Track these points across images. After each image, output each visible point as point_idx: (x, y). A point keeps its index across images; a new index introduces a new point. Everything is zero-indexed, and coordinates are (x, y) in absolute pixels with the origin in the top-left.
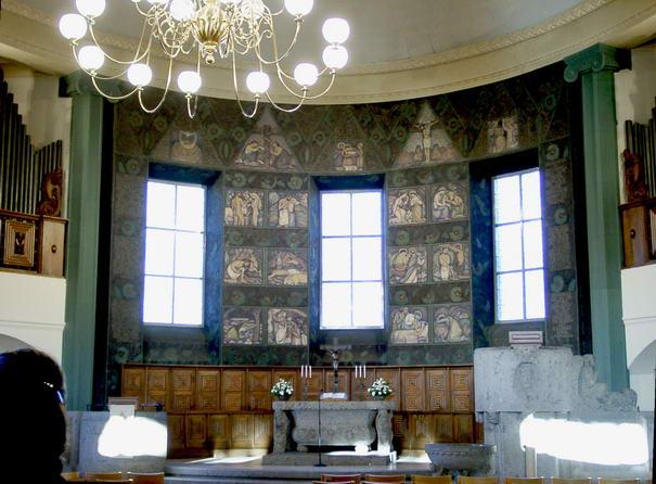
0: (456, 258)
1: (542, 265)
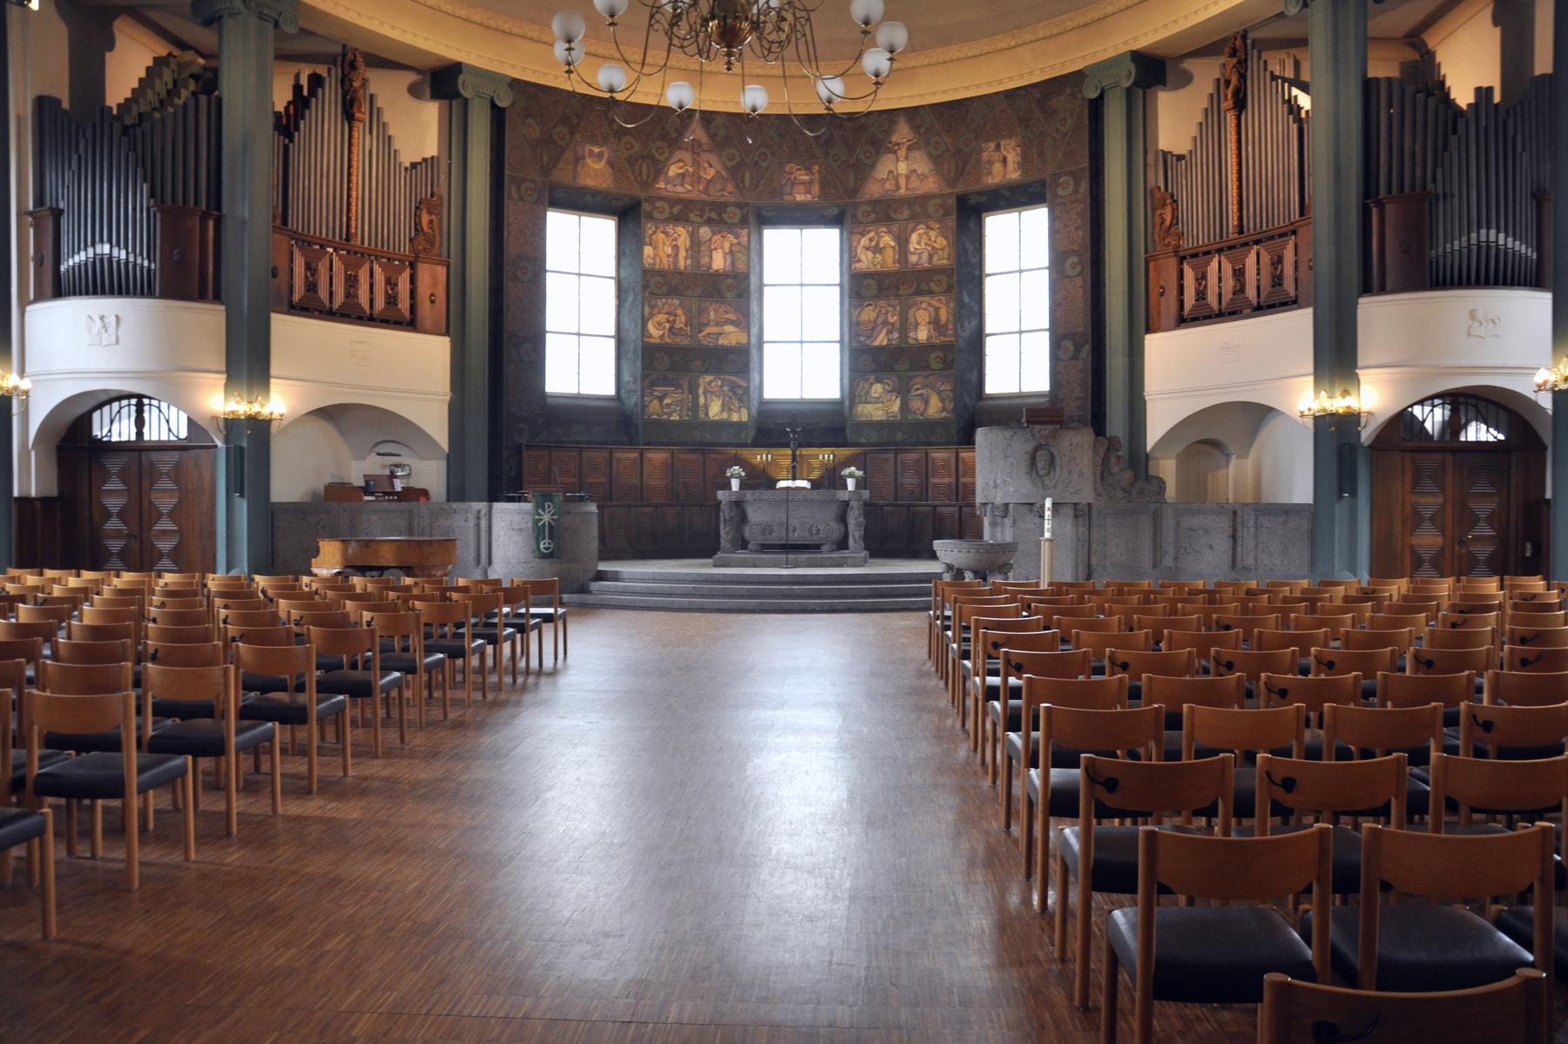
0: (937, 315)
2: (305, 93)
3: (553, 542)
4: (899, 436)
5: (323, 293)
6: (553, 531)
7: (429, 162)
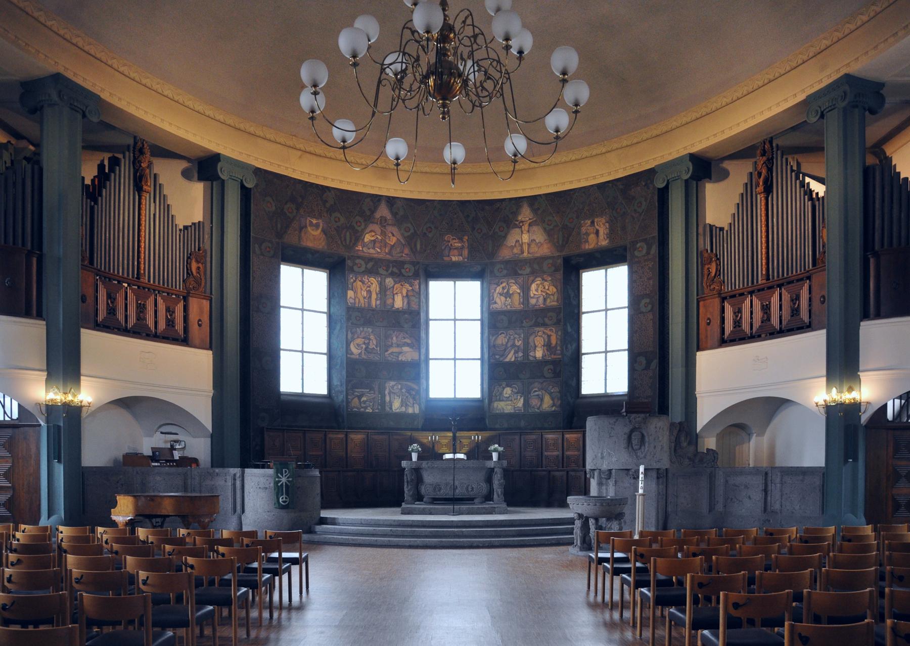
0: (549, 340)
1: (627, 347)
2: (107, 171)
3: (289, 498)
5: (120, 316)
6: (289, 490)
7: (197, 226)
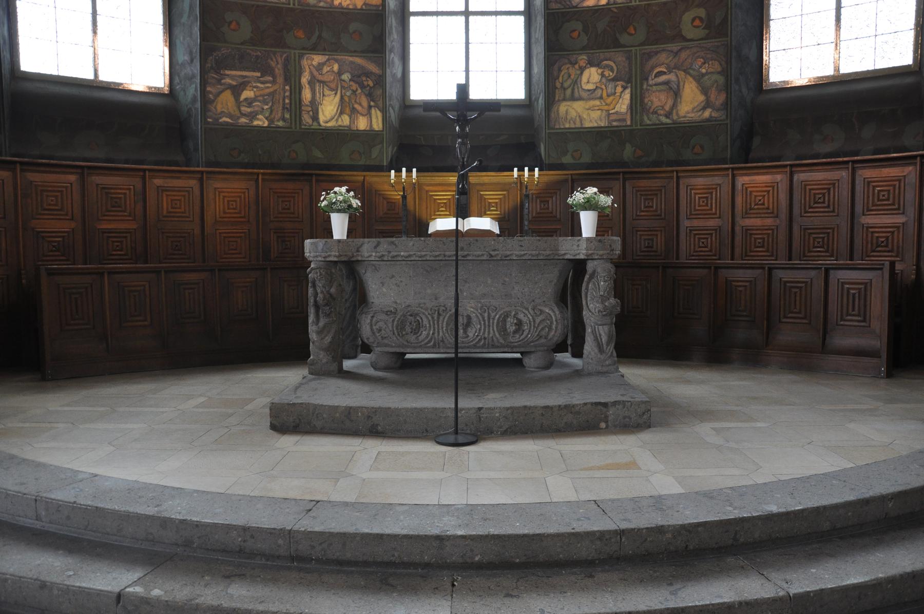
4: (628, 152)
